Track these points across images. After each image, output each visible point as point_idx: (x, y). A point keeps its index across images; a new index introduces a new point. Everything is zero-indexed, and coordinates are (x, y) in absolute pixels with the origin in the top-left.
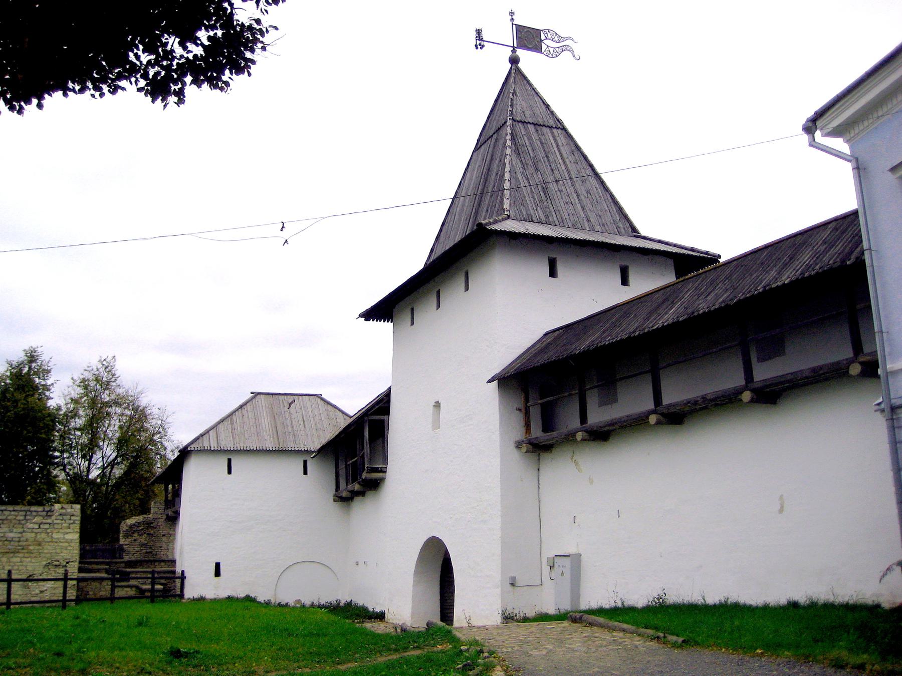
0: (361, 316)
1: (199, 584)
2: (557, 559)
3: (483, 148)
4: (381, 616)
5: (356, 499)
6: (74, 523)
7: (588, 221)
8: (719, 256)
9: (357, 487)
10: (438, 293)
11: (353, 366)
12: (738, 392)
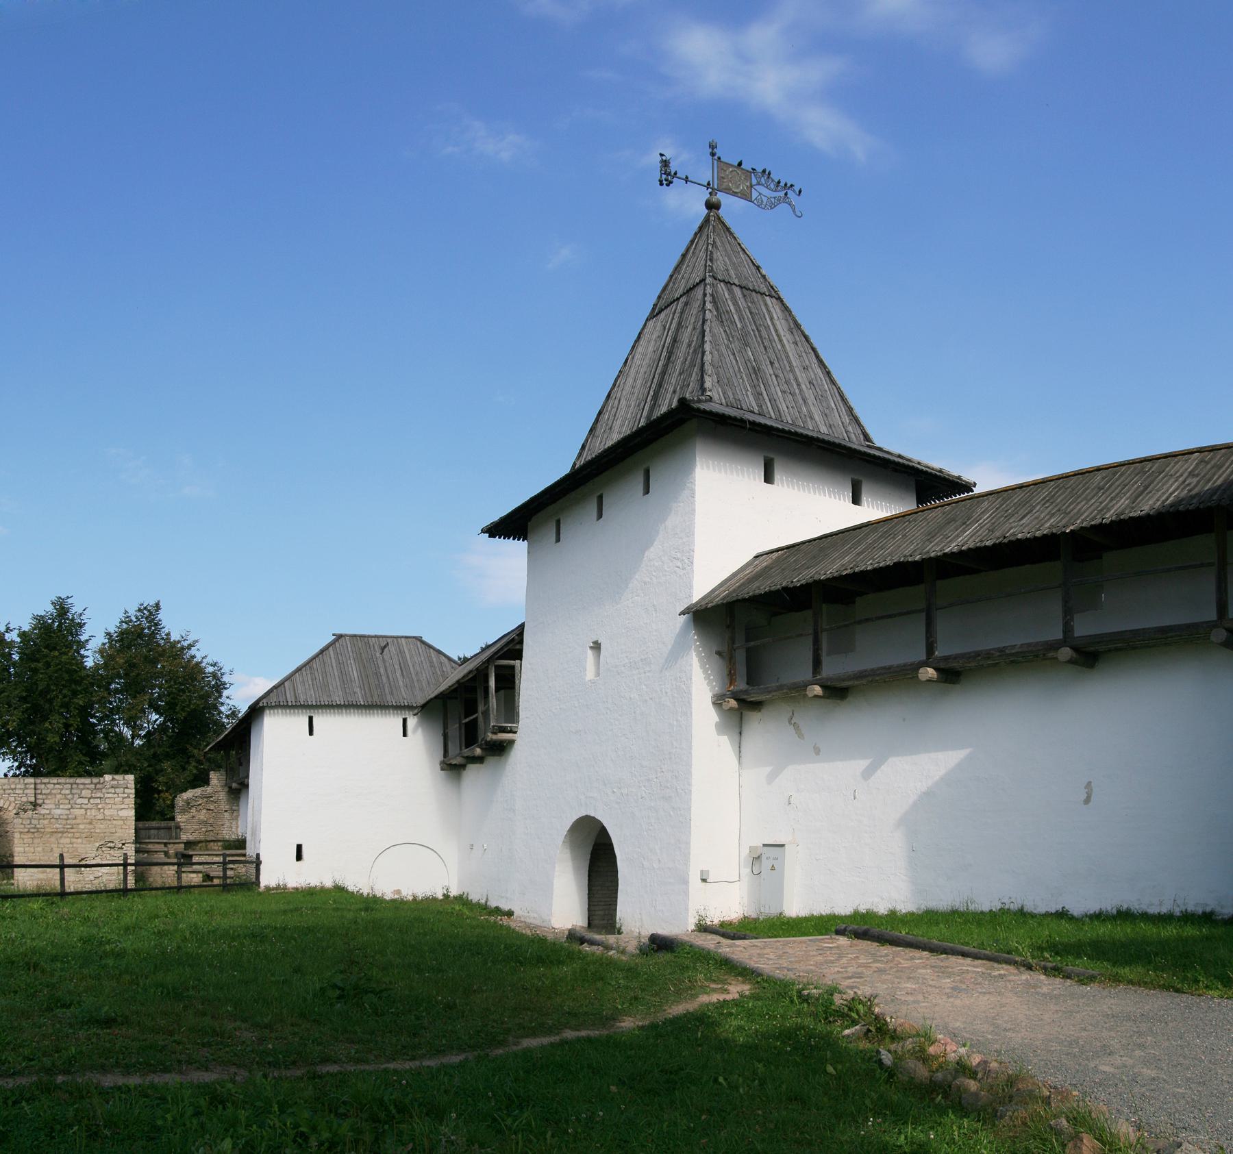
0: (483, 531)
3: (663, 315)
4: (510, 914)
7: (812, 418)
8: (975, 485)
9: (478, 751)
10: (600, 499)
11: (473, 596)
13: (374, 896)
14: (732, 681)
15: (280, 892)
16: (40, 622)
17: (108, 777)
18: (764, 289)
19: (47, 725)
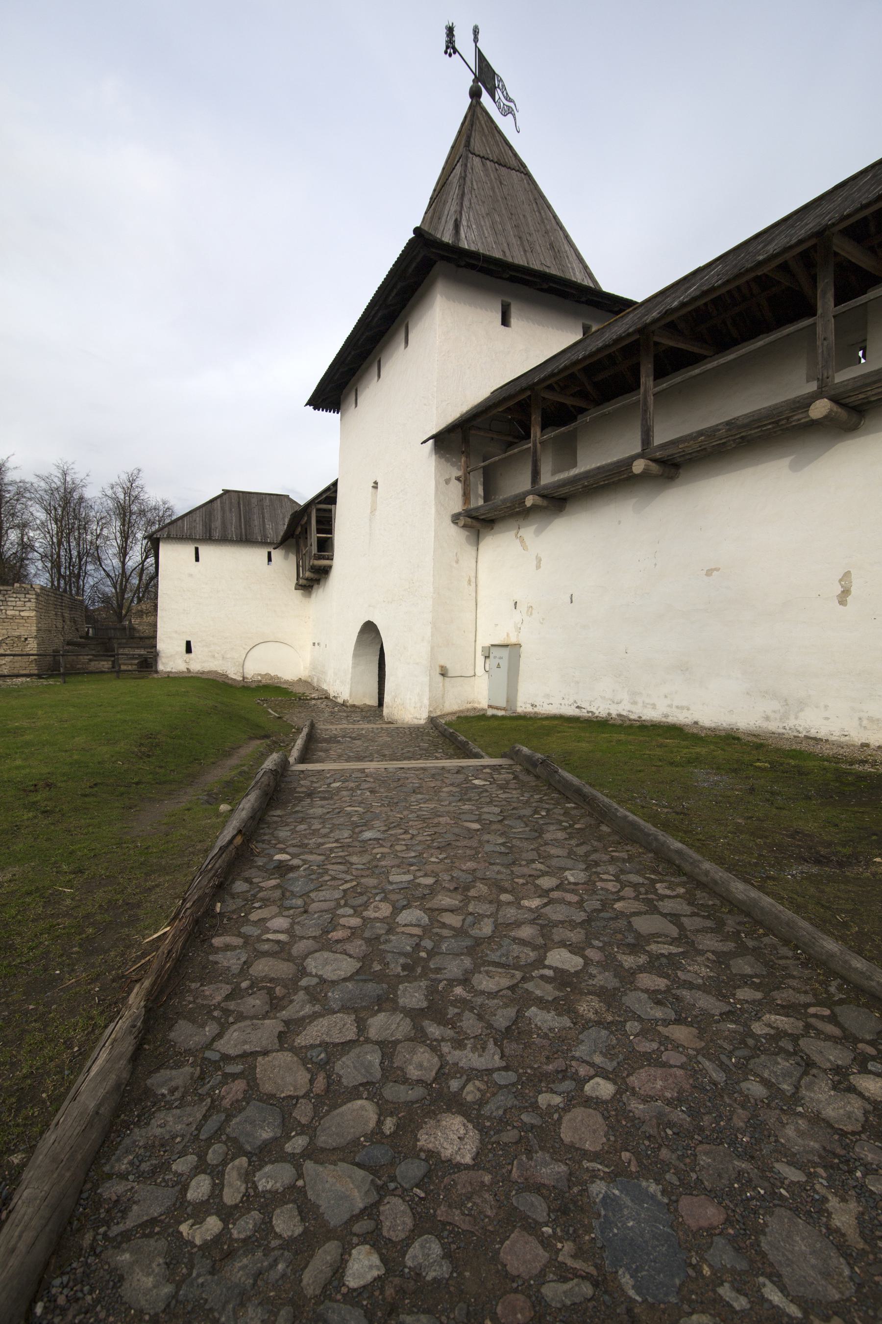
1: (171, 658)
2: (493, 650)
5: (315, 586)
6: (30, 601)
14: (465, 503)
15: (174, 679)
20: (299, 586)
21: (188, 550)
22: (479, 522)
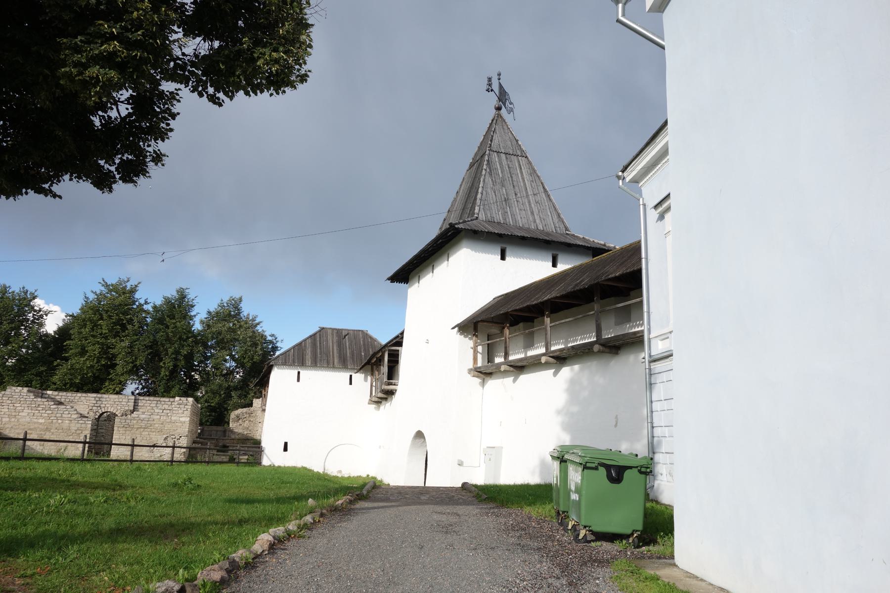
0: (388, 279)
1: (272, 456)
12: (591, 344)
13: (327, 475)
15: (274, 469)
16: (168, 301)
17: (177, 398)
18: (519, 153)
19: (161, 364)
20: (371, 402)
21: (292, 373)
22: (485, 373)
